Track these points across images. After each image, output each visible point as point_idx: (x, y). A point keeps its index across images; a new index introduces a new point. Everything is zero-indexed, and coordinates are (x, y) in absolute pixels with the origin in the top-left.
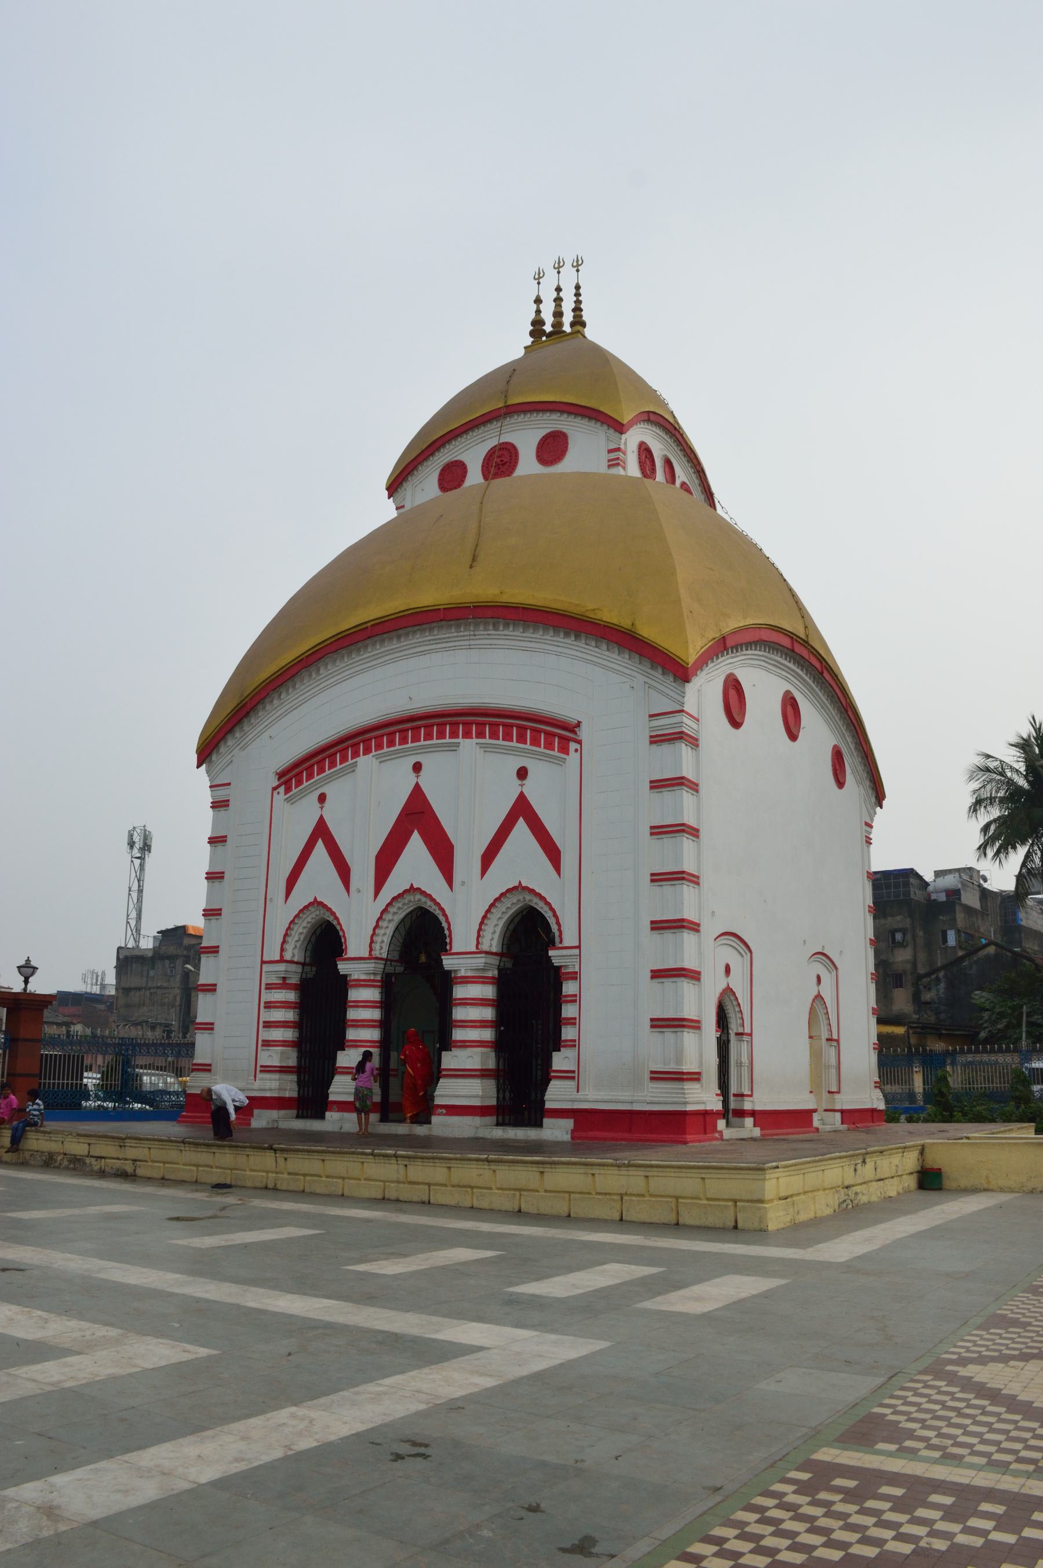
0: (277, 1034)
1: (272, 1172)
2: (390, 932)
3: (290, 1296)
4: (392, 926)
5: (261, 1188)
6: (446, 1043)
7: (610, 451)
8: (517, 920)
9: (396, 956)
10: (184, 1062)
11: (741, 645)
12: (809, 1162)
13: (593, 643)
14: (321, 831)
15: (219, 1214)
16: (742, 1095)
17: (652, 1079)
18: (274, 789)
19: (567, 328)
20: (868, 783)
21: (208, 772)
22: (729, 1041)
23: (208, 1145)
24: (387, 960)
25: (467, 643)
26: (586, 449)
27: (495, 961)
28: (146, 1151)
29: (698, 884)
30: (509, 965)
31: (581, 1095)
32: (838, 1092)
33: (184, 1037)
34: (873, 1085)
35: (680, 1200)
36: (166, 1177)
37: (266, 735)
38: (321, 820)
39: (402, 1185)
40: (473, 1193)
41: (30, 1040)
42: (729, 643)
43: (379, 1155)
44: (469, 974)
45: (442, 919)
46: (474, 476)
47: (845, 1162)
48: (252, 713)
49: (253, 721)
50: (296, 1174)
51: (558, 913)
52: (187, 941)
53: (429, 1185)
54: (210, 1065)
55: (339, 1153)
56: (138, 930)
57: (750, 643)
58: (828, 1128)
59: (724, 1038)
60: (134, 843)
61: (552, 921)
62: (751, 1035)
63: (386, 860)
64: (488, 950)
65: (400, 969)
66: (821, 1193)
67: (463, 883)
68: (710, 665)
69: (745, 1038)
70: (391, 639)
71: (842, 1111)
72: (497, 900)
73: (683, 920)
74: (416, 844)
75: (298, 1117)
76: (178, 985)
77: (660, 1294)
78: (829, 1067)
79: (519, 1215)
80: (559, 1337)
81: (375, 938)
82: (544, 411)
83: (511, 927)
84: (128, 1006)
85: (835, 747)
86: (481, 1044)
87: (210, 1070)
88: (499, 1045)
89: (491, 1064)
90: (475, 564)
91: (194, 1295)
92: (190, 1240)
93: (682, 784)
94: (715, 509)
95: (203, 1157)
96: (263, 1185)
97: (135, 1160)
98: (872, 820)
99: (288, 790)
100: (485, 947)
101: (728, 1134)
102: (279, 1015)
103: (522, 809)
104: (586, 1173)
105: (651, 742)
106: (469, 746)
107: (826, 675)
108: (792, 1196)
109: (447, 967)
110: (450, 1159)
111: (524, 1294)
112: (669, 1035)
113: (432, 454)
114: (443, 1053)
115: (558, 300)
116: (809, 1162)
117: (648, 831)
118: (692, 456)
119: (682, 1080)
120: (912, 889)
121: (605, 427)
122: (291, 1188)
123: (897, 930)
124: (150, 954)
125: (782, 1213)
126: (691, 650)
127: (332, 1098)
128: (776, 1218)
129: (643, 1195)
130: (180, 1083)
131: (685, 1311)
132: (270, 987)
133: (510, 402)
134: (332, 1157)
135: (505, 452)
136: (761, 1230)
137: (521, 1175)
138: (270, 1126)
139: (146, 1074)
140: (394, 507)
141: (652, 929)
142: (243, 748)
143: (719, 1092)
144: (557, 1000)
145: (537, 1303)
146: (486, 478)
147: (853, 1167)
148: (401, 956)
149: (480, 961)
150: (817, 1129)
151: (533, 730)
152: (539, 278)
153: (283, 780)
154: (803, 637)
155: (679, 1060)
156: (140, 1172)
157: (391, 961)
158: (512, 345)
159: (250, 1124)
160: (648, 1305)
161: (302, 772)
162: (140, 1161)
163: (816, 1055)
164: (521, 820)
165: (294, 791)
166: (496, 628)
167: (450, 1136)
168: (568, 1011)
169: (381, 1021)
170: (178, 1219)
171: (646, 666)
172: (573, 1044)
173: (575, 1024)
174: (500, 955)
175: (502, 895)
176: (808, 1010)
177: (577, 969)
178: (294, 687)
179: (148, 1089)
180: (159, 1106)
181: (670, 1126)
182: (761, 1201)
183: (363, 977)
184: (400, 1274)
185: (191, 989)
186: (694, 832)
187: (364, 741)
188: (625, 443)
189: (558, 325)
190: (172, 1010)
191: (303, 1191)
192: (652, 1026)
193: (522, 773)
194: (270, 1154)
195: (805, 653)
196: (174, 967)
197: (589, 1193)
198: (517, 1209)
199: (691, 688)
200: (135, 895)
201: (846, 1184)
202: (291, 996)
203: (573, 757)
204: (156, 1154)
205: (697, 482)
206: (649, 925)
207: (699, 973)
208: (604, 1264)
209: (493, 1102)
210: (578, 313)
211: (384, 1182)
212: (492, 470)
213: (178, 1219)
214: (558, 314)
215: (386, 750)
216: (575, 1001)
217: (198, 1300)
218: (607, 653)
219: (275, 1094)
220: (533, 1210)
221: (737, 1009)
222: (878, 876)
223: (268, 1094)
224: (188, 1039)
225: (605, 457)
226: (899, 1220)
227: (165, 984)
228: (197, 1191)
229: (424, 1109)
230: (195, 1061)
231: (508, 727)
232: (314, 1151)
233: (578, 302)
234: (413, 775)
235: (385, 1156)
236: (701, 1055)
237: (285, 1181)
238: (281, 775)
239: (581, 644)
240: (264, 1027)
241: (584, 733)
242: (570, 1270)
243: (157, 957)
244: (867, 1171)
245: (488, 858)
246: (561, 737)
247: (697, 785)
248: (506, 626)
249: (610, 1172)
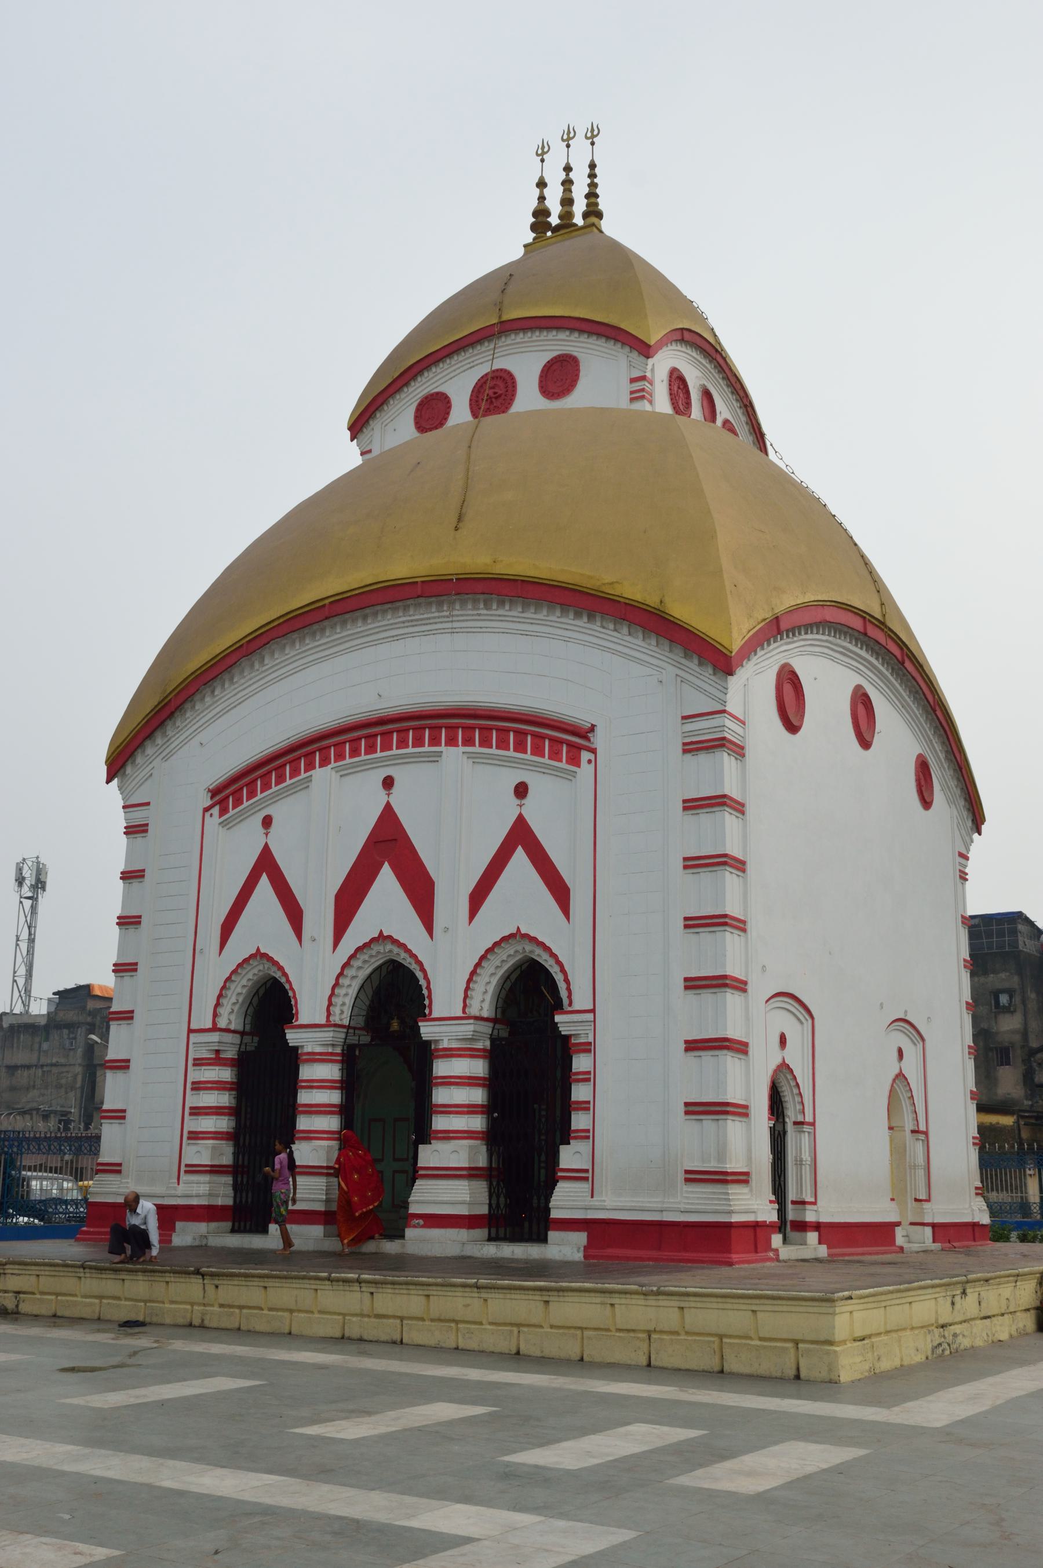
1: (199, 1304)
2: (353, 991)
3: (219, 1471)
4: (356, 985)
5: (184, 1326)
6: (424, 1134)
8: (514, 977)
9: (360, 1022)
10: (86, 1162)
11: (799, 627)
12: (891, 1292)
13: (611, 626)
14: (266, 864)
15: (129, 1361)
16: (803, 1203)
17: (687, 1180)
19: (578, 220)
20: (962, 803)
21: (120, 788)
22: (785, 1132)
23: (116, 1271)
24: (349, 1027)
25: (449, 625)
26: (603, 378)
27: (486, 1028)
28: (33, 1279)
29: (744, 930)
30: (504, 1034)
31: (595, 1202)
32: (928, 1200)
33: (87, 1128)
34: (974, 1191)
35: (725, 1340)
36: (59, 1314)
37: (195, 742)
38: (266, 849)
39: (366, 1319)
40: (457, 1330)
42: (783, 626)
43: (338, 1280)
44: (454, 1045)
45: (419, 975)
46: (460, 413)
47: (940, 1293)
48: (177, 714)
49: (178, 723)
50: (230, 1306)
51: (566, 968)
52: (91, 1005)
53: (402, 1319)
54: (120, 1165)
55: (286, 1278)
56: (28, 991)
57: (811, 625)
58: (915, 1247)
59: (779, 1128)
60: (24, 879)
61: (559, 978)
62: (813, 1124)
63: (349, 900)
64: (478, 1014)
65: (366, 1039)
66: (908, 1333)
67: (446, 930)
68: (760, 653)
69: (806, 1128)
70: (354, 620)
71: (934, 1226)
72: (489, 951)
73: (725, 977)
74: (386, 879)
75: (233, 1231)
76: (79, 1061)
77: (701, 1466)
78: (915, 1167)
79: (517, 1358)
80: (571, 1523)
81: (333, 1000)
82: (549, 328)
83: (508, 984)
84: (13, 1089)
85: (920, 756)
86: (469, 1135)
87: (119, 1172)
88: (492, 1137)
89: (482, 1162)
90: (461, 524)
91: (92, 1472)
92: (88, 1398)
93: (724, 804)
94: (766, 454)
95: (109, 1285)
96: (186, 1321)
97: (19, 1293)
98: (968, 850)
99: (223, 811)
100: (474, 1010)
101: (786, 1252)
103: (521, 835)
104: (602, 1304)
105: (685, 751)
106: (453, 756)
107: (908, 664)
108: (870, 1336)
110: (430, 1285)
111: (524, 1465)
112: (709, 1124)
113: (407, 384)
114: (420, 1146)
115: (567, 183)
116: (891, 1292)
117: (680, 863)
118: (738, 386)
119: (725, 1182)
120: (1020, 938)
121: (627, 349)
122: (223, 1325)
123: (1003, 991)
124: (43, 1022)
125: (858, 1359)
126: (735, 634)
128: (850, 1365)
129: (677, 1333)
130: (80, 1189)
131: (734, 1490)
132: (199, 1062)
133: (505, 318)
134: (276, 1283)
135: (499, 383)
136: (830, 1382)
137: (521, 1306)
138: (197, 1243)
139: (36, 1178)
140: (359, 452)
141: (686, 988)
142: (166, 759)
143: (773, 1198)
144: (566, 1078)
145: (541, 1476)
146: (475, 415)
147: (949, 1300)
148: (367, 1022)
149: (467, 1028)
150: (902, 1248)
151: (535, 735)
152: (544, 153)
154: (879, 616)
155: (722, 1155)
156: (24, 1308)
157: (355, 1028)
158: (509, 241)
159: (170, 1241)
160: (684, 1480)
161: (242, 789)
162: (24, 1293)
163: (898, 1152)
164: (520, 848)
165: (232, 812)
166: (487, 607)
167: (429, 1254)
168: (579, 1092)
169: (341, 1106)
170: (72, 1370)
171: (678, 655)
172: (586, 1135)
173: (588, 1109)
174: (494, 1021)
175: (496, 944)
176: (887, 1094)
177: (591, 1039)
178: (231, 679)
179: (38, 1198)
180: (54, 1223)
181: (711, 1242)
182: (831, 1343)
183: (318, 1049)
184: (364, 1438)
185: (96, 1066)
186: (739, 865)
187: (320, 750)
188: (653, 370)
189: (566, 216)
190: (72, 1094)
191: (239, 1329)
192: (687, 1113)
193: (521, 791)
194: (197, 1280)
195: (881, 637)
196: (75, 1038)
197: (608, 1330)
198: (514, 1351)
199: (735, 682)
200: (24, 946)
201: (941, 1321)
202: (226, 1074)
203: (585, 770)
204: (47, 1282)
205: (743, 419)
206: (682, 984)
207: (746, 1044)
208: (628, 1424)
209: (484, 1210)
210: (593, 200)
211: (344, 1315)
212: (483, 405)
213: (72, 1370)
214: (567, 202)
215: (348, 760)
216: (588, 1080)
217: (97, 1480)
218: (628, 638)
219: (204, 1202)
220: (535, 1352)
221: (796, 1091)
222: (976, 921)
223: (195, 1202)
224: (92, 1131)
225: (626, 388)
226: (1015, 1372)
227: (62, 1061)
228: (99, 1331)
229: (394, 1219)
230: (101, 1160)
231: (503, 732)
232: (253, 1276)
233: (593, 185)
234: (383, 793)
235: (346, 1281)
236: (749, 1150)
237: (215, 1316)
238: (214, 792)
239: (596, 626)
240: (191, 1114)
241: (599, 740)
242: (584, 1431)
243: (52, 1025)
244: (969, 1305)
245: (478, 898)
246: (570, 745)
247: (743, 805)
248: (501, 604)
249: (634, 1302)
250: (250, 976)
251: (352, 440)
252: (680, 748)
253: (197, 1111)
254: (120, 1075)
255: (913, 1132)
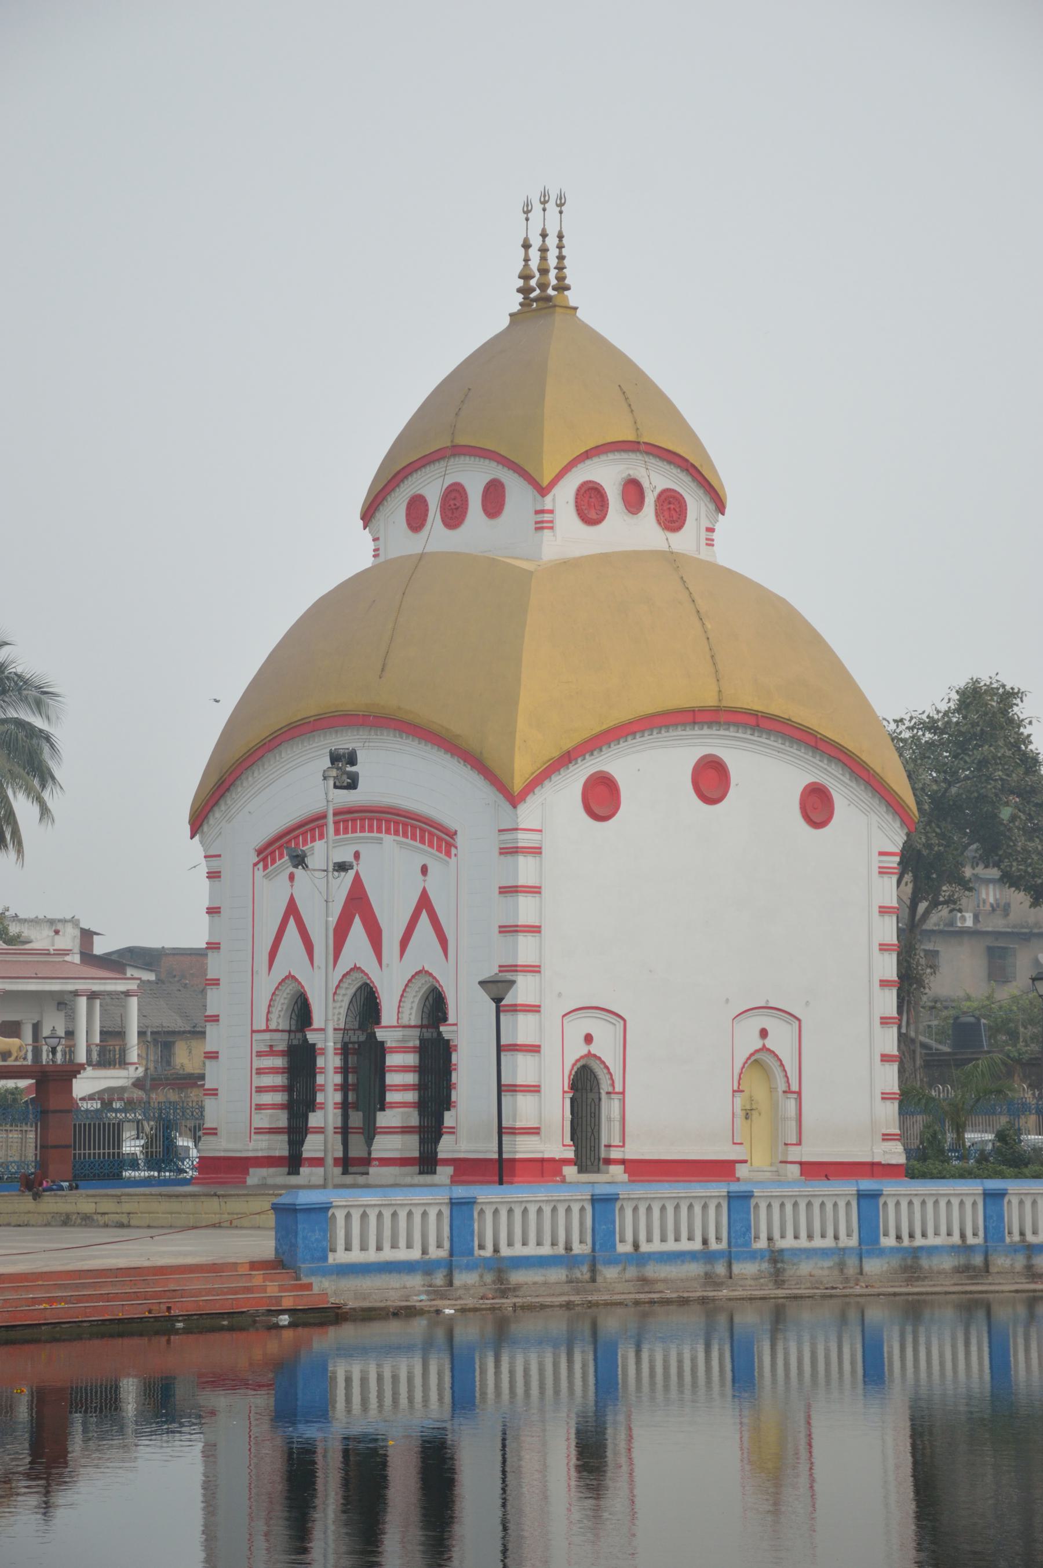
0: (267, 1098)
7: (537, 512)
18: (255, 865)
22: (600, 1099)
41: (61, 1111)
54: (216, 1129)
67: (388, 965)
71: (801, 1163)
87: (216, 1134)
102: (268, 1080)
109: (379, 1039)
127: (305, 1155)
132: (259, 1054)
142: (229, 821)
153: (261, 856)
159: (245, 1182)
178: (263, 765)
194: (216, 1199)
202: (279, 1062)
209: (416, 1154)
219: (265, 1154)
223: (260, 1154)
238: (259, 852)
241: (460, 840)
250: (288, 991)
251: (365, 528)
252: (497, 851)
253: (260, 1090)
254: (214, 1062)
255: (784, 1092)
